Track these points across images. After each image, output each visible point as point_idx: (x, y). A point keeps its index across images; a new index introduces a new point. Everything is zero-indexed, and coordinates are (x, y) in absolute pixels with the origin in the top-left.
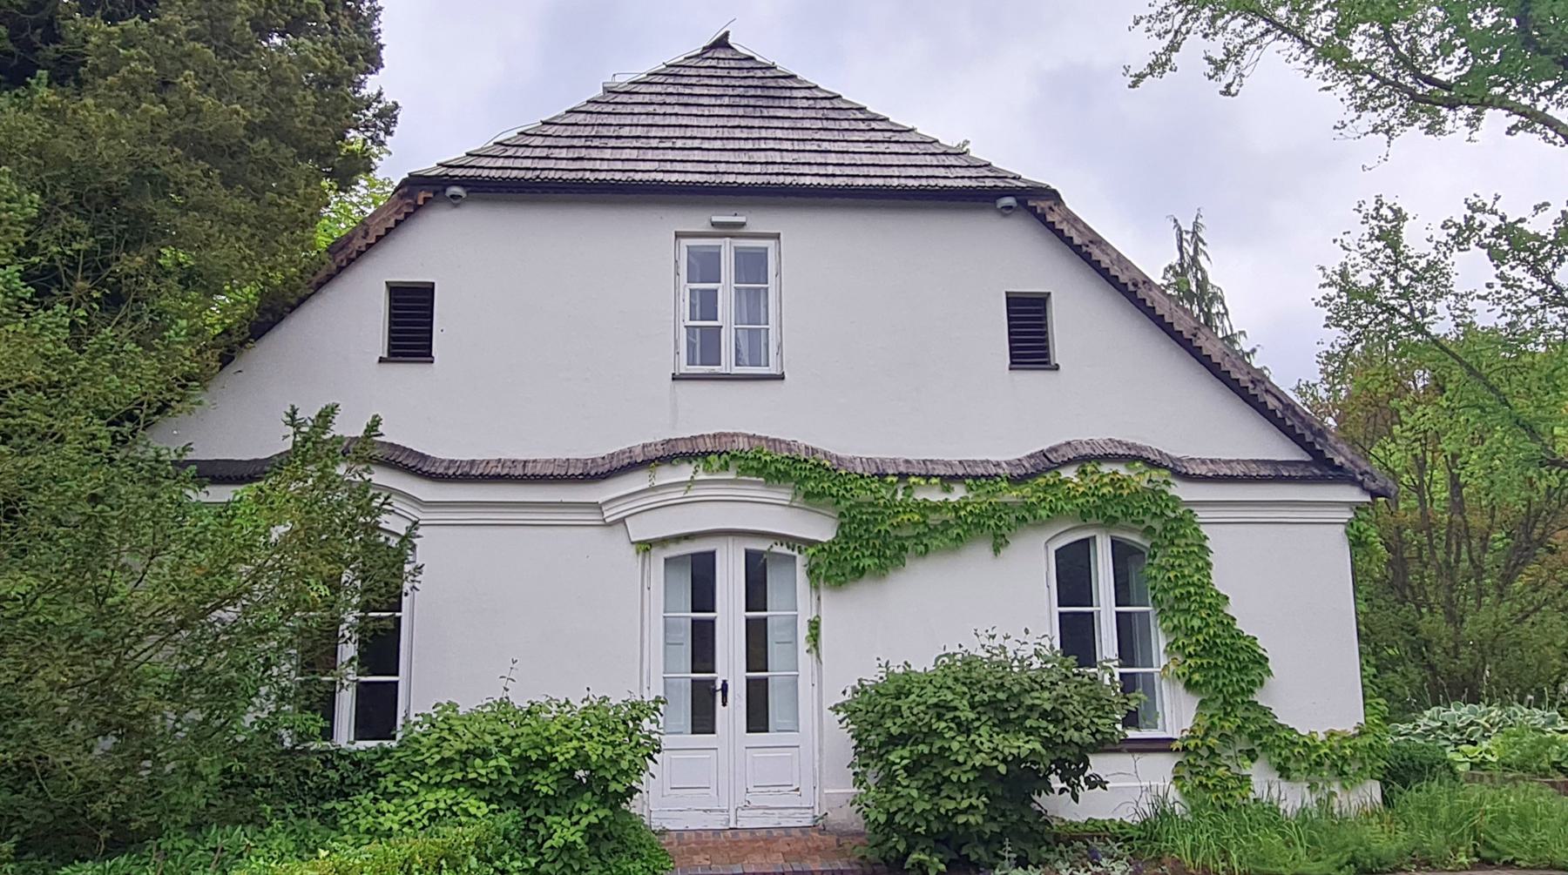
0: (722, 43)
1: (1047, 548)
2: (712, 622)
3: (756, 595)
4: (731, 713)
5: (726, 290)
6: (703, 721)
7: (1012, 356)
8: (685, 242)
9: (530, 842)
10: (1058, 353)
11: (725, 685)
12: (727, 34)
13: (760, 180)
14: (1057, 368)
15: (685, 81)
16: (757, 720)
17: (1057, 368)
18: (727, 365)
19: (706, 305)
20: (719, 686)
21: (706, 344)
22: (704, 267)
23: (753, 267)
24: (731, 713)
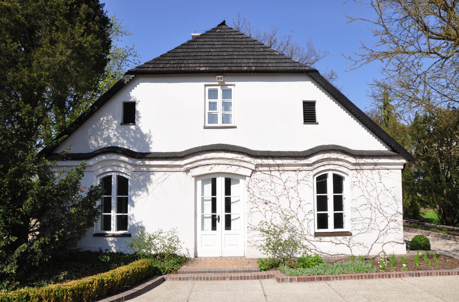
0: (223, 23)
1: (313, 178)
2: (334, 210)
3: (228, 191)
4: (221, 224)
5: (219, 101)
6: (214, 227)
7: (304, 119)
8: (207, 88)
9: (4, 238)
10: (318, 119)
11: (219, 216)
12: (224, 21)
13: (292, 68)
14: (317, 124)
15: (211, 37)
16: (228, 226)
17: (317, 124)
18: (220, 124)
19: (213, 106)
20: (217, 217)
21: (212, 118)
22: (213, 94)
23: (227, 94)
24: (221, 224)
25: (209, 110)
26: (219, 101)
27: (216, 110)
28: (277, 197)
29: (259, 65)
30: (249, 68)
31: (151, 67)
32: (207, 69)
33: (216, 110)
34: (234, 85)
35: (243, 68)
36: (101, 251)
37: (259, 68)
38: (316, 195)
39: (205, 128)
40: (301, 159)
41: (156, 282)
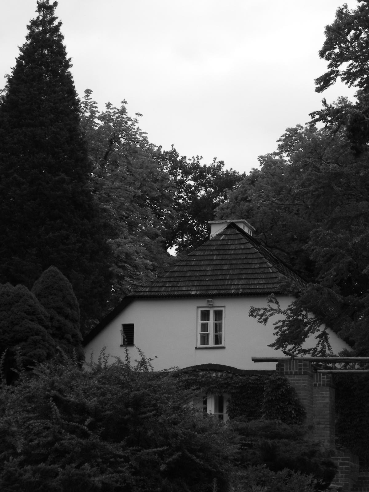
19: (205, 327)
21: (205, 339)
22: (205, 315)
23: (219, 315)
25: (208, 323)
26: (211, 322)
27: (221, 344)
28: (131, 226)
29: (247, 287)
30: (237, 291)
31: (147, 290)
32: (198, 293)
33: (221, 344)
34: (224, 307)
35: (230, 292)
36: (102, 474)
37: (246, 291)
38: (223, 333)
39: (196, 348)
40: (273, 359)
41: (205, 323)
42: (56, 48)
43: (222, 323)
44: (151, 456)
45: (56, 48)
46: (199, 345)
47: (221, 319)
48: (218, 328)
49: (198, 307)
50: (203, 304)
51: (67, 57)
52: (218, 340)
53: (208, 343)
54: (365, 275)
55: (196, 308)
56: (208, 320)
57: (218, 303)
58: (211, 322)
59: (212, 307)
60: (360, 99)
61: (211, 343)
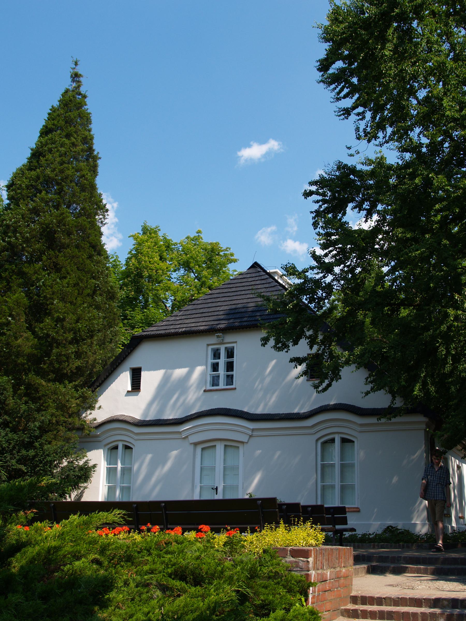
21: (215, 381)
22: (216, 355)
23: (230, 353)
34: (236, 342)
42: (343, 196)
43: (233, 362)
44: (140, 610)
45: (343, 196)
46: (209, 387)
47: (232, 357)
48: (230, 366)
49: (208, 345)
50: (212, 340)
51: (95, 153)
52: (230, 379)
53: (218, 385)
54: (403, 317)
55: (206, 345)
56: (219, 358)
57: (229, 338)
58: (222, 362)
59: (222, 343)
60: (239, 157)
61: (222, 385)
